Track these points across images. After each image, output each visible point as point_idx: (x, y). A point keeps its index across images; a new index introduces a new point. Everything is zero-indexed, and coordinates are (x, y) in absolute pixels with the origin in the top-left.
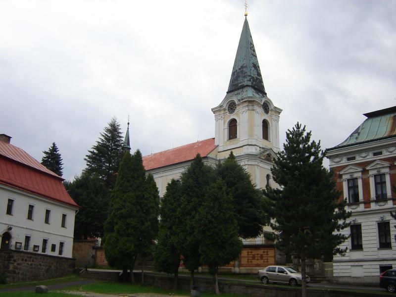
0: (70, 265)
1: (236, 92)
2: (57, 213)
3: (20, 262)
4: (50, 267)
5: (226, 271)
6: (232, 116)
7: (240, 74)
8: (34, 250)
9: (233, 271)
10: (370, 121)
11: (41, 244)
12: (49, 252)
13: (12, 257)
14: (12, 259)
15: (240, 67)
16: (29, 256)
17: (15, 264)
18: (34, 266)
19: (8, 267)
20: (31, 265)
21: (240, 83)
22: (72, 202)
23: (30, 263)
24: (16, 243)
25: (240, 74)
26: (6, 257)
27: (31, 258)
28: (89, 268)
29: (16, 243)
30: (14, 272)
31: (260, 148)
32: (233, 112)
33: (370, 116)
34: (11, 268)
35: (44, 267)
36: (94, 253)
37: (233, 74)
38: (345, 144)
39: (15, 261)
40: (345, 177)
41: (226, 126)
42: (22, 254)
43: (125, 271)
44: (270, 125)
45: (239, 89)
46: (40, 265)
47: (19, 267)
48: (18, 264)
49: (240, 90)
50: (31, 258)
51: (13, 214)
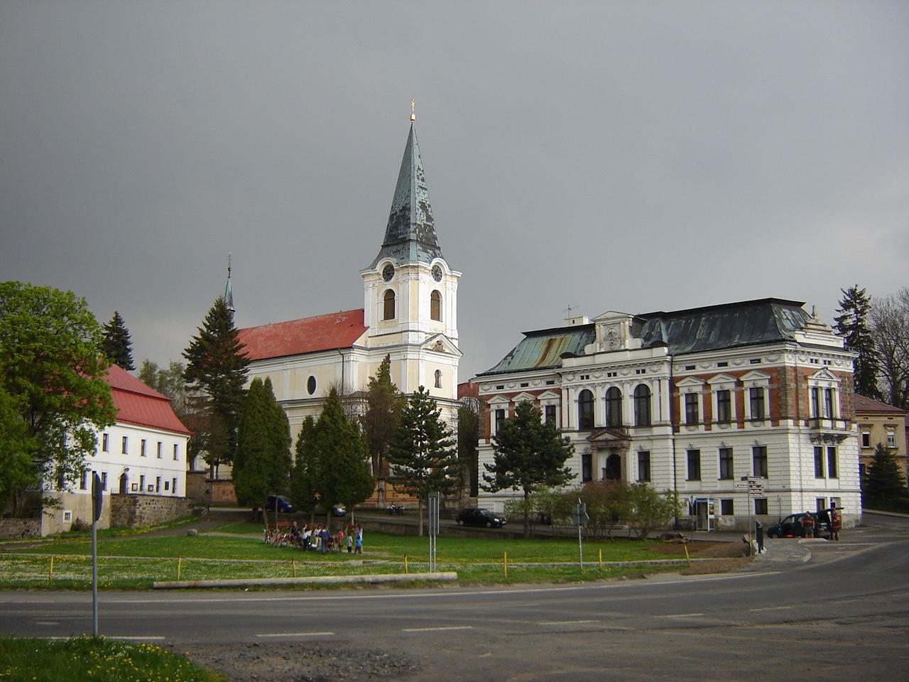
0: (189, 505)
1: (395, 248)
2: (169, 440)
3: (145, 506)
4: (171, 508)
5: (369, 506)
6: (389, 286)
7: (401, 220)
8: (149, 490)
9: (376, 506)
10: (528, 340)
11: (154, 483)
12: (163, 492)
13: (137, 501)
14: (138, 504)
15: (401, 208)
16: (152, 498)
17: (141, 509)
18: (156, 509)
19: (134, 513)
20: (154, 508)
21: (401, 234)
22: (185, 430)
23: (153, 507)
24: (133, 484)
25: (401, 220)
26: (132, 501)
27: (153, 500)
28: (249, 512)
29: (149, 486)
30: (141, 517)
31: (426, 333)
32: (390, 279)
33: (530, 335)
34: (137, 514)
35: (165, 510)
36: (208, 488)
37: (392, 217)
38: (495, 371)
39: (140, 505)
40: (494, 407)
41: (382, 299)
42: (146, 498)
43: (255, 509)
44: (444, 297)
45: (398, 244)
46: (162, 507)
47: (144, 511)
48: (144, 509)
49: (400, 245)
50: (153, 500)
51: (109, 450)
